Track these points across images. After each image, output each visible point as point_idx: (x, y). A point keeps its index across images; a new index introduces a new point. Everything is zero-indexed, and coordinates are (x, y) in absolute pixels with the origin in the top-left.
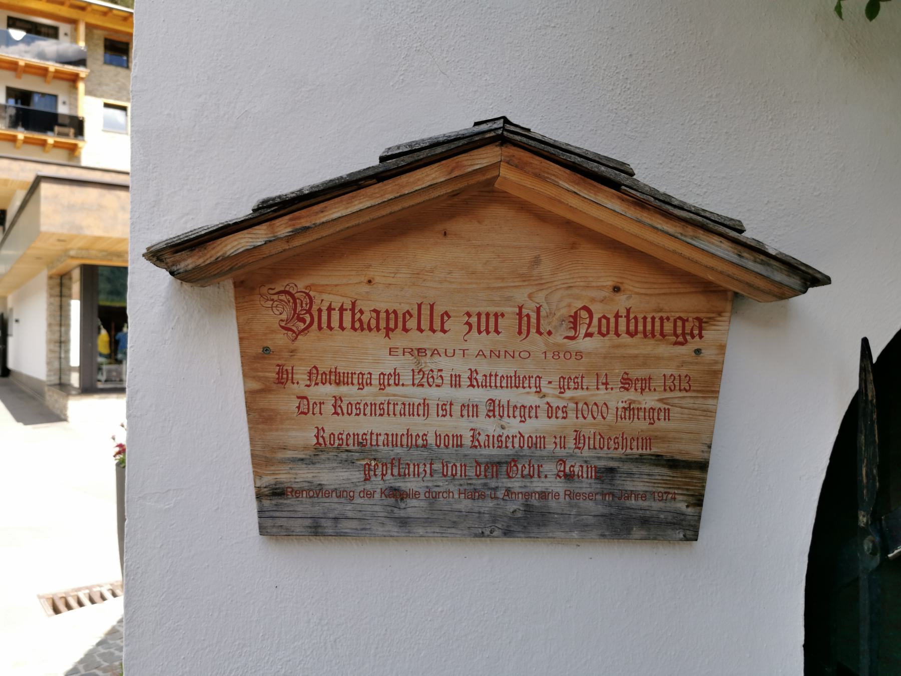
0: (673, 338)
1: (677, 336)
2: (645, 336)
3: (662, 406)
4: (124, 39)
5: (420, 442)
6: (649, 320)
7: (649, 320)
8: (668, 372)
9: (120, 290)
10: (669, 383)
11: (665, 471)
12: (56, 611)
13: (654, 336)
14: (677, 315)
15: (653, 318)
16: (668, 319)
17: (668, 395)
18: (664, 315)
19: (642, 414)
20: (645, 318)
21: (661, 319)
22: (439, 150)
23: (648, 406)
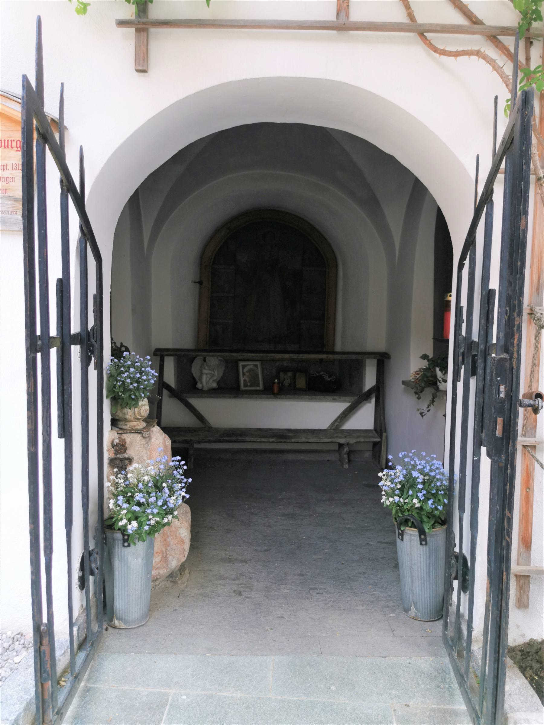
0: (16, 149)
1: (17, 148)
2: (5, 147)
3: (12, 176)
4: (113, 428)
5: (434, 491)
6: (6, 141)
7: (6, 141)
8: (14, 163)
9: (124, 623)
10: (14, 167)
11: (13, 202)
12: (145, 71)
13: (8, 147)
14: (18, 139)
15: (8, 141)
16: (14, 141)
17: (14, 171)
18: (13, 139)
19: (3, 179)
20: (5, 140)
21: (11, 141)
22: (234, 438)
23: (6, 176)
